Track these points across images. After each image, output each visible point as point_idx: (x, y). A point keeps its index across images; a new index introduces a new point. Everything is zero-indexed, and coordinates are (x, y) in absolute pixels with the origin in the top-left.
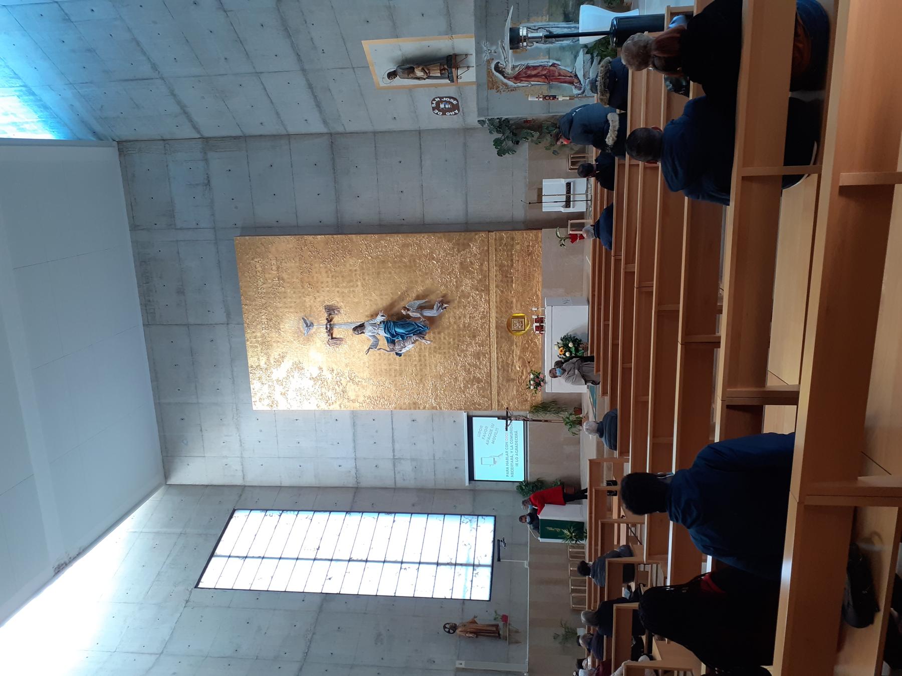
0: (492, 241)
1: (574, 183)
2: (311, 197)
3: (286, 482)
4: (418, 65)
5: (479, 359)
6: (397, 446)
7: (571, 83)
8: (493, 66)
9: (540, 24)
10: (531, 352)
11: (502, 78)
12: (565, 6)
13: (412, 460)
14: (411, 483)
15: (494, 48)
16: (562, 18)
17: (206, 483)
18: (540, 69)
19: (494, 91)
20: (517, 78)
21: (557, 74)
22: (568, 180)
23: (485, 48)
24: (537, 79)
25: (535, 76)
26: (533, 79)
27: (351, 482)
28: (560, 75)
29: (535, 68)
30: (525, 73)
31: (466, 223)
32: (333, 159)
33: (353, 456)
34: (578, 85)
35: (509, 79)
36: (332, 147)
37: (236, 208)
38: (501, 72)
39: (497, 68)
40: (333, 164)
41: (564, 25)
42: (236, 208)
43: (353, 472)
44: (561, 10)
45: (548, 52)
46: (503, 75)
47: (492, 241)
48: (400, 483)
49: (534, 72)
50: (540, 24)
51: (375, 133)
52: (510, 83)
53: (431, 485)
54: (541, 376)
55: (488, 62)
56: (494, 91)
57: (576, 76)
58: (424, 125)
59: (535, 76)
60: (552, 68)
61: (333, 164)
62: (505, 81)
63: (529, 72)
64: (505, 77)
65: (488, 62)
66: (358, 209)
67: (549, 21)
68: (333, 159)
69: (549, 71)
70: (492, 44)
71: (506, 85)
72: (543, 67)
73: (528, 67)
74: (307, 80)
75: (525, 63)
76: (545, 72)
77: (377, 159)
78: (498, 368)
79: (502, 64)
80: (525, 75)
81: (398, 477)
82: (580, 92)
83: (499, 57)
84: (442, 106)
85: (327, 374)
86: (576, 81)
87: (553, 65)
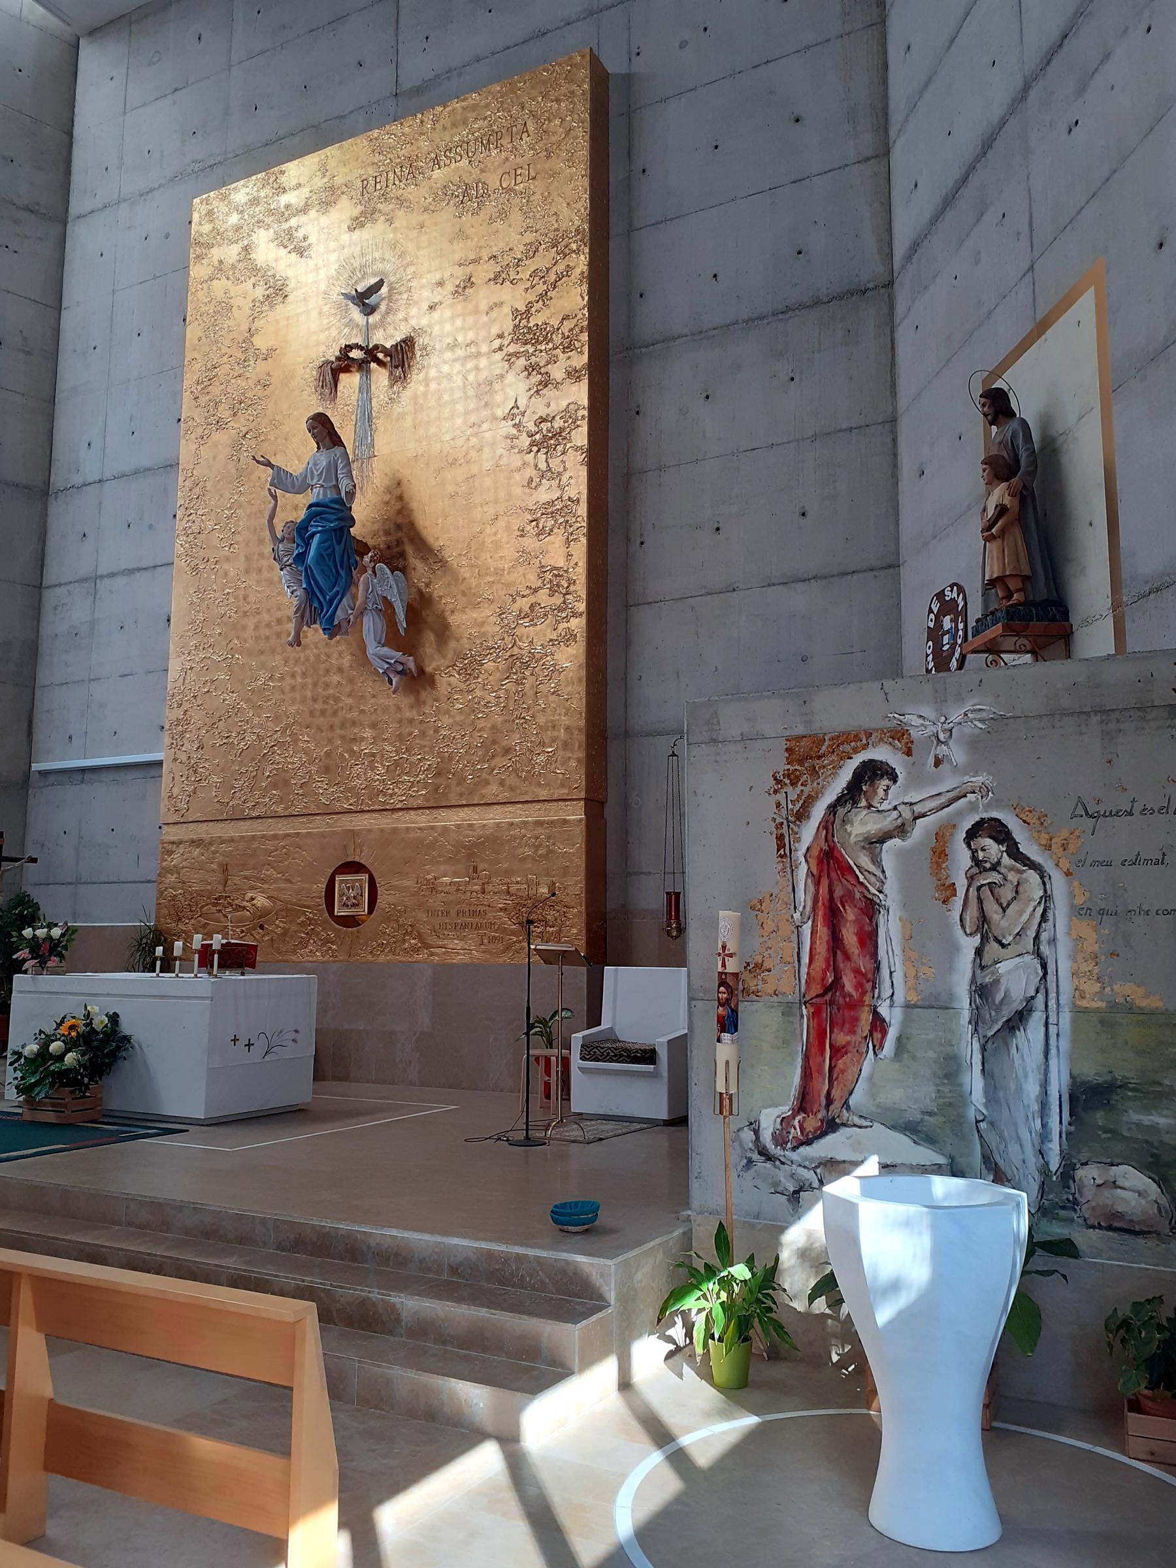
0: (554, 813)
1: (655, 1075)
2: (706, 254)
3: (68, 320)
4: (1024, 496)
5: (274, 786)
6: (121, 581)
7: (803, 1104)
8: (881, 753)
9: (1065, 966)
10: (285, 932)
11: (830, 797)
12: (1152, 1094)
13: (92, 624)
14: (54, 624)
15: (957, 753)
16: (1091, 1072)
17: (78, 131)
18: (864, 964)
19: (782, 766)
20: (829, 861)
21: (841, 1038)
22: (663, 1054)
23: (956, 716)
24: (822, 948)
25: (836, 942)
26: (823, 932)
27: (58, 479)
28: (837, 1052)
29: (869, 939)
30: (848, 897)
31: (627, 734)
32: (817, 303)
33: (108, 474)
34: (795, 1132)
35: (827, 825)
36: (851, 293)
37: (683, 45)
38: (853, 793)
39: (872, 772)
40: (802, 307)
41: (1059, 1082)
42: (683, 45)
43: (78, 480)
44: (1127, 1067)
45: (940, 1004)
46: (840, 801)
47: (554, 813)
48: (51, 598)
49: (849, 937)
50: (1065, 966)
51: (892, 421)
52: (808, 832)
53: (43, 676)
54: (54, 962)
55: (899, 736)
56: (782, 766)
57: (831, 1126)
58: (908, 576)
59: (836, 942)
60: (866, 1018)
61: (802, 307)
62: (818, 811)
63: (850, 914)
64: (833, 808)
65: (899, 736)
66: (678, 406)
67: (1079, 1012)
68: (817, 303)
69: (855, 1005)
70: (973, 744)
71: (802, 815)
72: (870, 979)
73: (871, 909)
74: (1002, 123)
75: (892, 897)
76: (848, 983)
77: (814, 438)
78: (253, 838)
79: (891, 796)
80: (843, 904)
81: (63, 590)
82: (767, 1137)
83: (917, 780)
84: (947, 623)
85: (257, 369)
86: (812, 1123)
87: (879, 1025)
